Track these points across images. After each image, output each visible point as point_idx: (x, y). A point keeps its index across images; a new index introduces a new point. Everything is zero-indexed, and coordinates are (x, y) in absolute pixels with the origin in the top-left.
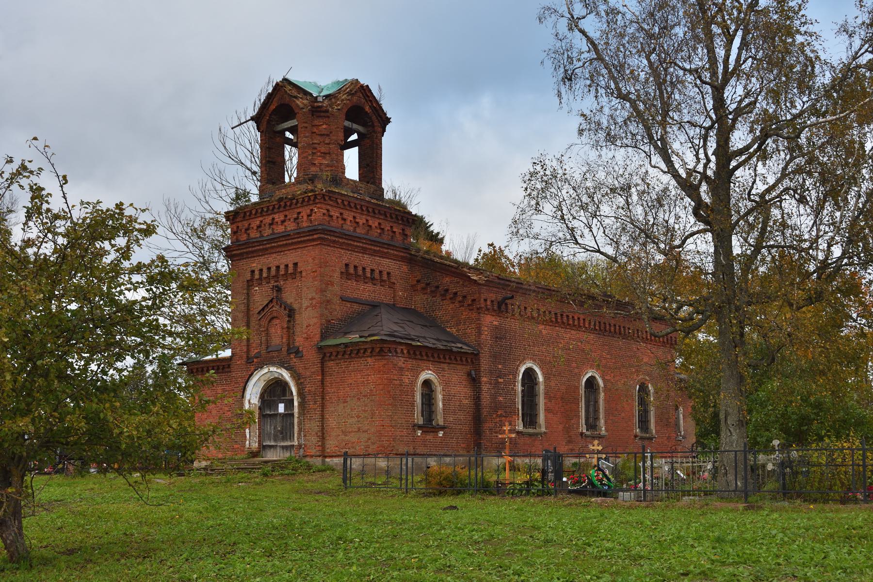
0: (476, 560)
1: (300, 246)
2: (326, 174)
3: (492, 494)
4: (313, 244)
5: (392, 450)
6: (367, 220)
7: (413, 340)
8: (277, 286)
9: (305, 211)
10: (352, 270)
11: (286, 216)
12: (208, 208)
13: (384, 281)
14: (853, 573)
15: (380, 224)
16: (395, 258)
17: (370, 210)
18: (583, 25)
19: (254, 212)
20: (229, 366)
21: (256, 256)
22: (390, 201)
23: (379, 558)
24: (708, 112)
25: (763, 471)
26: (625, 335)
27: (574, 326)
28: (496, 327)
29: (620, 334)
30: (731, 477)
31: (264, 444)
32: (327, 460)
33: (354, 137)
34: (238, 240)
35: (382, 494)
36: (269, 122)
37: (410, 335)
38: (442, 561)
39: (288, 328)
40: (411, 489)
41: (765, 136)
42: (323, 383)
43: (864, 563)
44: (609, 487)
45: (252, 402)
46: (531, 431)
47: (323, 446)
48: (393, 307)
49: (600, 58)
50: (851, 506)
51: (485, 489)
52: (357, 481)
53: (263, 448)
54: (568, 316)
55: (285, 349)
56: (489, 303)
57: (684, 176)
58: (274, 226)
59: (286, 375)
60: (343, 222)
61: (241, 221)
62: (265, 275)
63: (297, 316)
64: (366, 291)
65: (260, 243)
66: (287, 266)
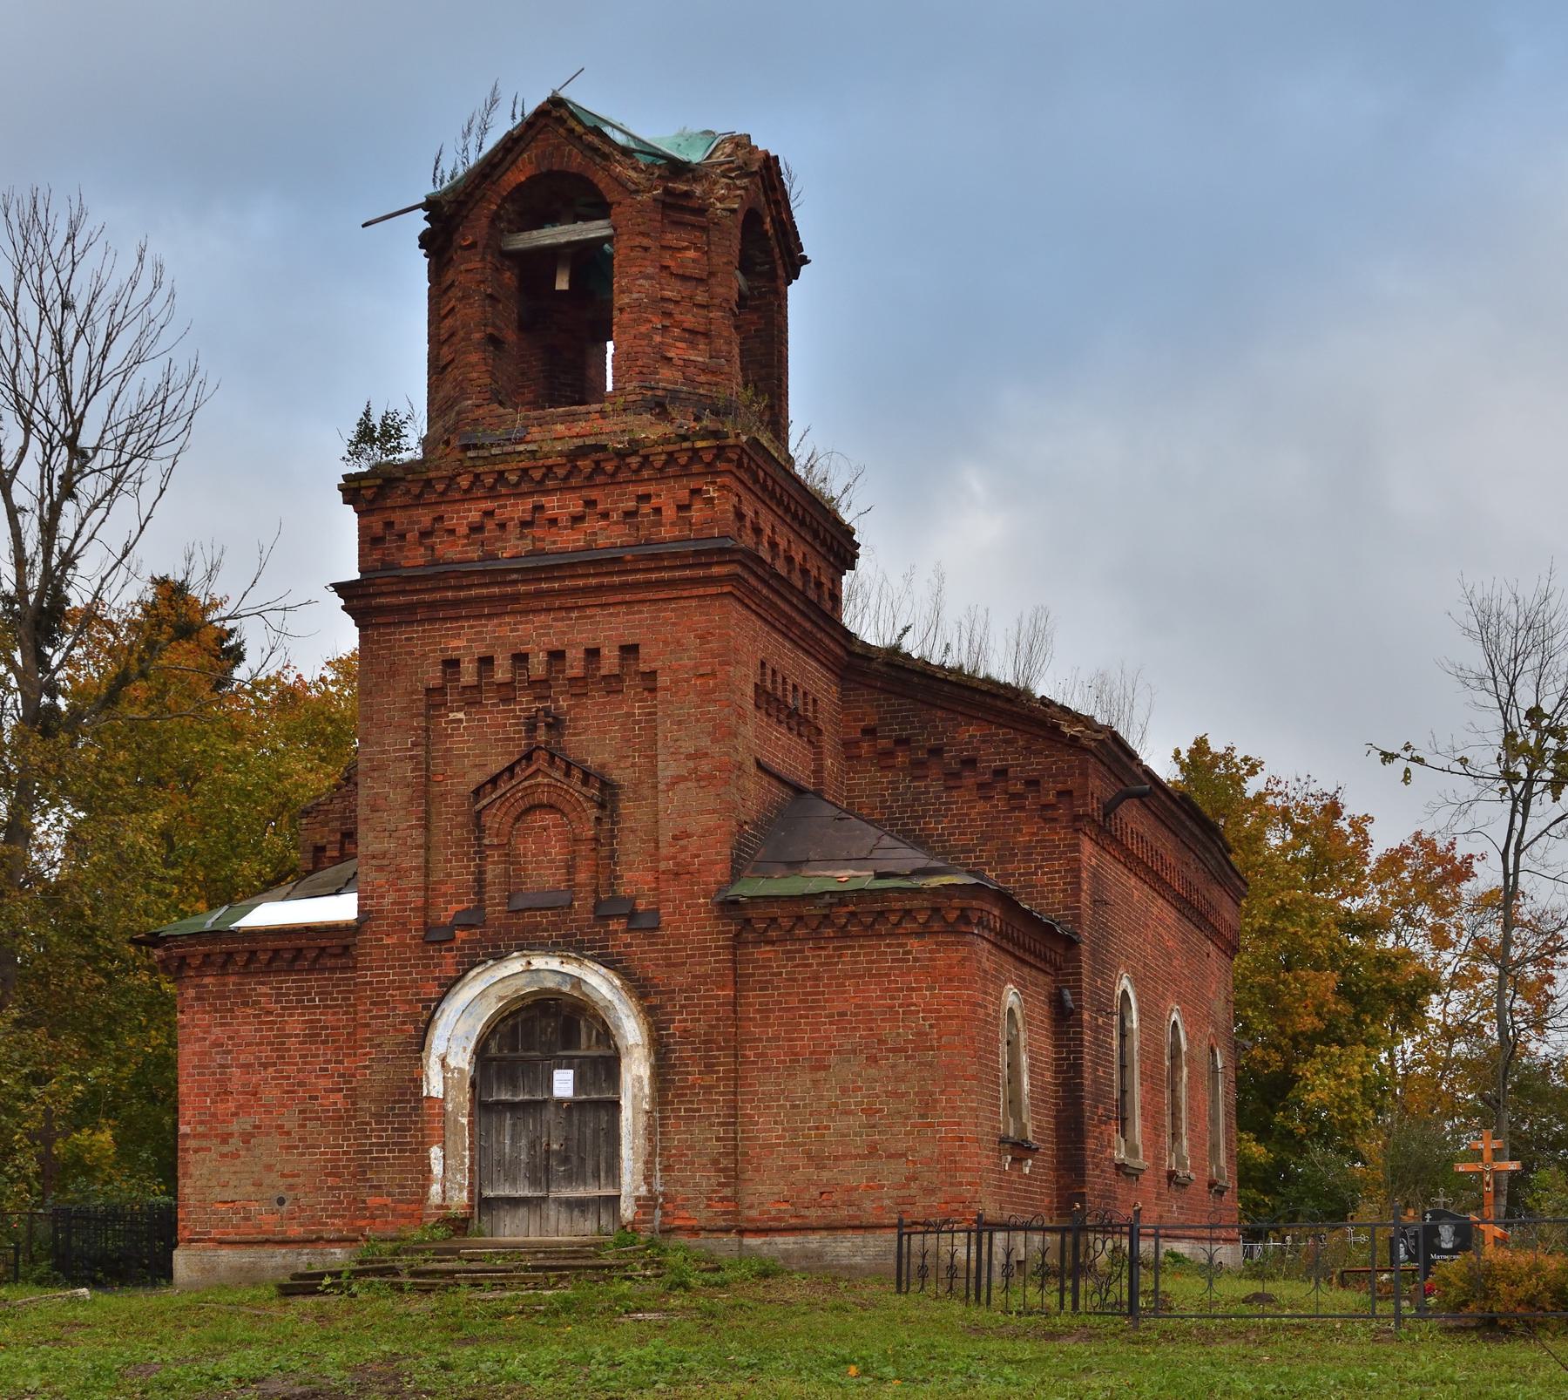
1: (651, 596)
4: (701, 591)
21: (467, 618)
31: (488, 1193)
32: (752, 1241)
45: (451, 1062)
59: (600, 984)
61: (405, 507)
63: (626, 807)
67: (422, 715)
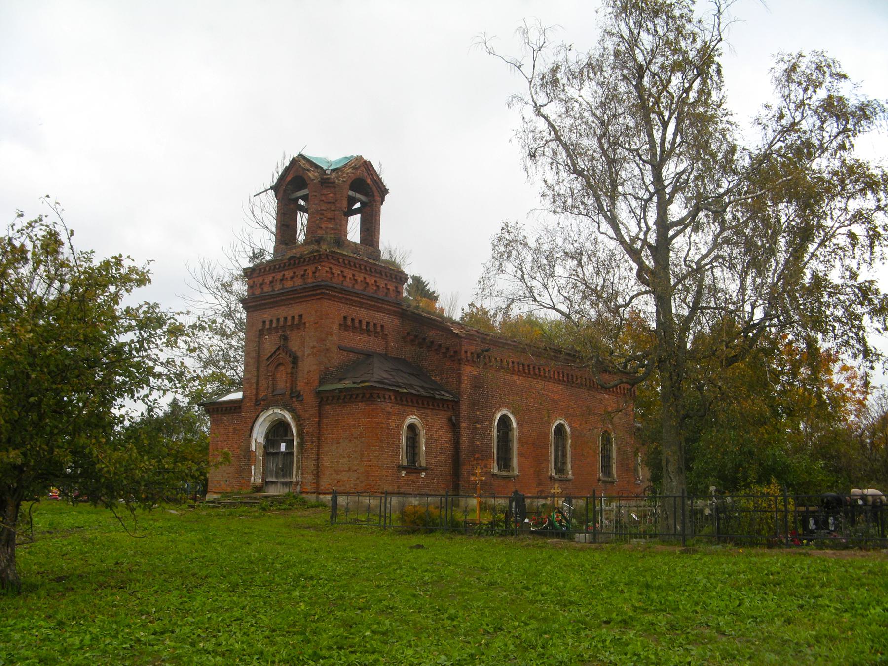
0: (420, 602)
2: (330, 237)
3: (460, 533)
5: (378, 489)
6: (365, 278)
7: (400, 387)
8: (284, 336)
9: (310, 269)
10: (349, 322)
11: (294, 273)
12: (237, 266)
13: (378, 333)
14: (762, 621)
15: (375, 281)
16: (389, 312)
17: (368, 269)
18: (544, 110)
19: (267, 269)
20: (240, 407)
22: (386, 262)
23: (330, 597)
24: (647, 187)
25: (702, 515)
26: (590, 386)
27: (560, 380)
28: (476, 377)
29: (586, 386)
30: (671, 522)
32: (321, 497)
33: (358, 205)
34: (253, 294)
35: (362, 531)
36: (285, 191)
37: (398, 382)
38: (385, 603)
39: (292, 373)
40: (389, 527)
41: (697, 209)
42: (319, 426)
43: (774, 610)
44: (568, 528)
45: (258, 440)
46: (505, 473)
47: (317, 484)
48: (385, 357)
49: (558, 138)
50: (775, 550)
51: (456, 528)
52: (341, 518)
53: (266, 483)
54: (539, 368)
55: (288, 393)
56: (469, 354)
57: (628, 241)
58: (284, 282)
59: (288, 417)
60: (343, 279)
62: (274, 325)
63: (300, 364)
64: (360, 341)
65: (272, 296)
66: (293, 317)
67: (712, 273)
